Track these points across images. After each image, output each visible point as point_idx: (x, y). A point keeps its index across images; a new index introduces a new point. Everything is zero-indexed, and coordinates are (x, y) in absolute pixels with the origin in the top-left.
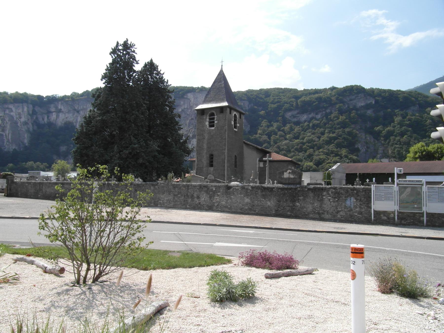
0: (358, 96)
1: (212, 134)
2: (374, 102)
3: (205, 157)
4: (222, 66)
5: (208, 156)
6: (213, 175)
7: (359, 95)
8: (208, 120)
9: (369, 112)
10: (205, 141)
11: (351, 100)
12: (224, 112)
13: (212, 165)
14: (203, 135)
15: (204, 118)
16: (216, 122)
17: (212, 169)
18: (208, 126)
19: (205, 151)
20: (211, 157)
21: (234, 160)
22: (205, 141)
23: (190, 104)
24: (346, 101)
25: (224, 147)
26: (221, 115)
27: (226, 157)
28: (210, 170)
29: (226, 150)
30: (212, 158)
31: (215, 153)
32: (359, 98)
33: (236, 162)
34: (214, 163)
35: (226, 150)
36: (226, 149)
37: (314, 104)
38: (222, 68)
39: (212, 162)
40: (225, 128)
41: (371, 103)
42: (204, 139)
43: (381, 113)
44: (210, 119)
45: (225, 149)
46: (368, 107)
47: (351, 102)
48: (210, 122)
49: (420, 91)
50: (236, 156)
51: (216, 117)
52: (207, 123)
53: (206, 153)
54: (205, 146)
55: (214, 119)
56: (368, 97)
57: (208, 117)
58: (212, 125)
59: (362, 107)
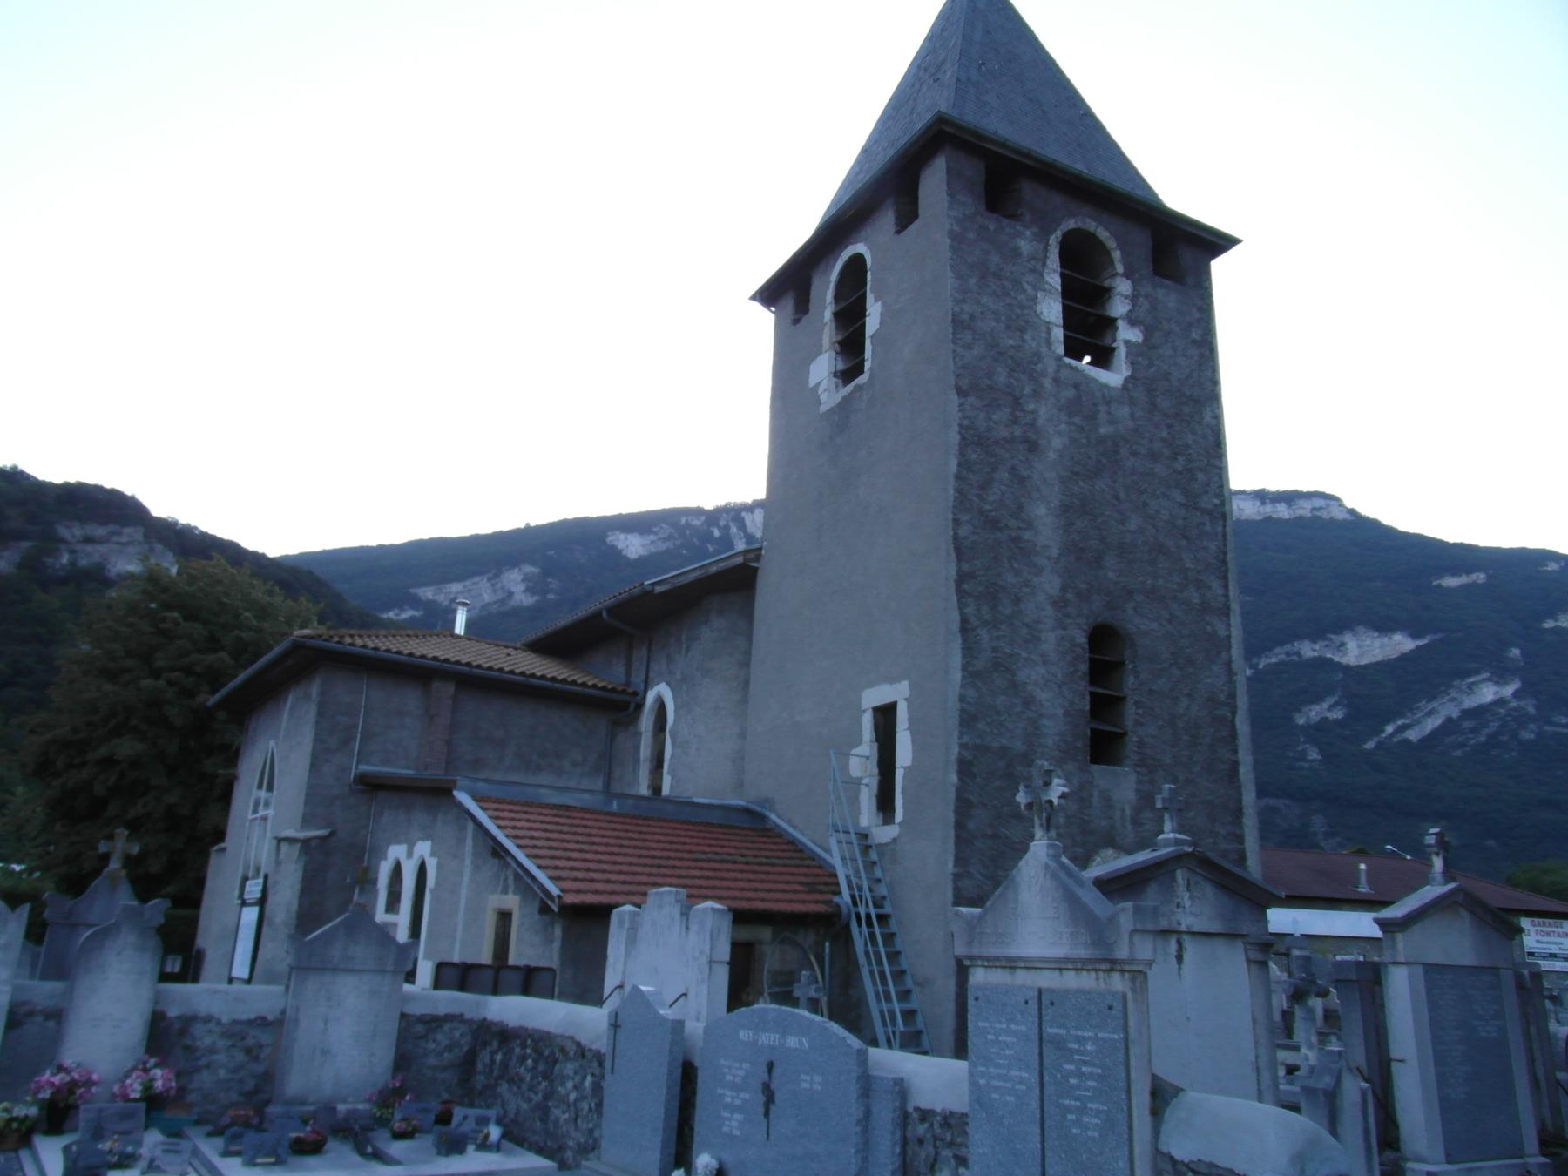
0: (120, 534)
3: (1050, 640)
7: (127, 530)
10: (1047, 471)
11: (88, 540)
13: (1103, 746)
14: (1016, 402)
19: (1050, 584)
20: (1104, 653)
22: (1047, 471)
24: (68, 536)
28: (1107, 801)
29: (1236, 620)
31: (1144, 625)
32: (124, 539)
35: (1236, 620)
37: (1450, 582)
42: (1033, 447)
45: (1225, 611)
47: (89, 548)
54: (1044, 525)
56: (159, 547)
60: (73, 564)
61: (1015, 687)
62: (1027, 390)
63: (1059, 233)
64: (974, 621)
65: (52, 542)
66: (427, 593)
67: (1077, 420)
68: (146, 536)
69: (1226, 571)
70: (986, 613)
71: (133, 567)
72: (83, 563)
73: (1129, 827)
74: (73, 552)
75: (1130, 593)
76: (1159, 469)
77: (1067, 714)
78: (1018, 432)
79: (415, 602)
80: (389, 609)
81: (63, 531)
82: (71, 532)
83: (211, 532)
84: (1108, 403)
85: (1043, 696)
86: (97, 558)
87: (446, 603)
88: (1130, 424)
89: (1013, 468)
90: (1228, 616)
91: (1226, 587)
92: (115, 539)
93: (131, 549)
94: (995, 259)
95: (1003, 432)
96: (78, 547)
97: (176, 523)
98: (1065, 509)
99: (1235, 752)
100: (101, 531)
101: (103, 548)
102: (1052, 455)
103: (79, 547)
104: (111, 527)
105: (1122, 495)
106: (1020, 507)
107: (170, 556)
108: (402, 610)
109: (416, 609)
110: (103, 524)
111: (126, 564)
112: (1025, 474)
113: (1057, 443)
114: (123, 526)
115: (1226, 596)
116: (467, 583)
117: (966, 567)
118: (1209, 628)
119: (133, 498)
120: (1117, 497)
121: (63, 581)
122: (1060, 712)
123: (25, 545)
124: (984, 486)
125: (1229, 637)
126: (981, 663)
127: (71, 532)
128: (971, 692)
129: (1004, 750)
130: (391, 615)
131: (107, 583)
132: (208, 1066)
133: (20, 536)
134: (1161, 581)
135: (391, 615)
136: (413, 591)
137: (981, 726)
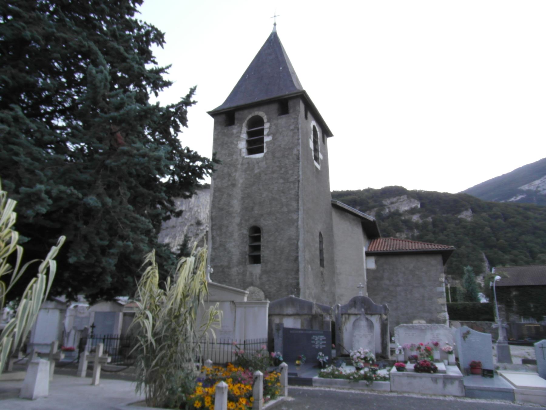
0: (400, 199)
1: (257, 171)
2: (419, 206)
3: (236, 235)
4: (275, 24)
5: (246, 232)
6: (261, 287)
7: (402, 197)
8: (244, 136)
9: (415, 218)
10: (238, 192)
11: (392, 203)
12: (291, 111)
13: (256, 260)
14: (230, 175)
15: (235, 131)
16: (267, 139)
17: (257, 269)
18: (244, 151)
19: (237, 220)
20: (255, 234)
21: (317, 245)
23: (189, 206)
24: (387, 204)
25: (294, 204)
26: (283, 120)
27: (301, 231)
28: (251, 274)
30: (258, 239)
31: (265, 224)
32: (402, 200)
33: (321, 251)
34: (265, 253)
35: (301, 212)
36: (301, 208)
38: (275, 29)
39: (257, 248)
40: (295, 152)
41: (417, 207)
42: (234, 185)
43: (430, 219)
44: (250, 134)
46: (413, 211)
47: (393, 205)
48: (249, 142)
49: (469, 194)
50: (320, 234)
51: (267, 126)
52: (242, 145)
53: (240, 225)
54: (236, 205)
55: (261, 132)
56: (412, 200)
57: (245, 130)
58: (255, 145)
59: (406, 211)
60: (390, 211)
61: (225, 249)
62: (233, 170)
63: (246, 121)
64: (215, 236)
65: (383, 206)
66: (525, 187)
67: (248, 172)
68: (408, 197)
69: (298, 198)
70: (218, 233)
71: (407, 208)
72: (392, 210)
73: (258, 280)
74: (389, 208)
75: (262, 215)
76: (275, 176)
77: (240, 253)
78: (230, 183)
79: (522, 192)
80: (512, 197)
81: (384, 202)
82: (386, 202)
83: (428, 190)
84: (258, 163)
85: (233, 250)
86: (396, 208)
87: (535, 189)
88: (265, 166)
89: (228, 193)
90: (298, 212)
91: (298, 203)
92: (399, 201)
93: (404, 202)
94: (226, 139)
95: (226, 185)
96: (392, 206)
97: (416, 190)
98: (243, 198)
99: (298, 253)
100: (394, 200)
101: (396, 205)
102: (239, 185)
103: (390, 206)
104: (397, 197)
105: (261, 188)
106: (229, 203)
107: (416, 201)
108: (517, 196)
109: (522, 195)
110: (395, 197)
111: (404, 208)
112: (231, 193)
113: (241, 181)
114: (401, 196)
115: (298, 206)
116: (542, 179)
117: (214, 223)
118: (290, 218)
119: (395, 186)
120: (260, 189)
121: (388, 217)
122: (238, 253)
123: (375, 209)
124: (219, 201)
125: (298, 218)
126: (216, 246)
127: (386, 202)
128: (214, 253)
129: (222, 266)
130: (513, 199)
131: (400, 215)
132: (243, 356)
133: (373, 207)
134: (273, 209)
135: (513, 199)
136: (519, 188)
137: (216, 261)
